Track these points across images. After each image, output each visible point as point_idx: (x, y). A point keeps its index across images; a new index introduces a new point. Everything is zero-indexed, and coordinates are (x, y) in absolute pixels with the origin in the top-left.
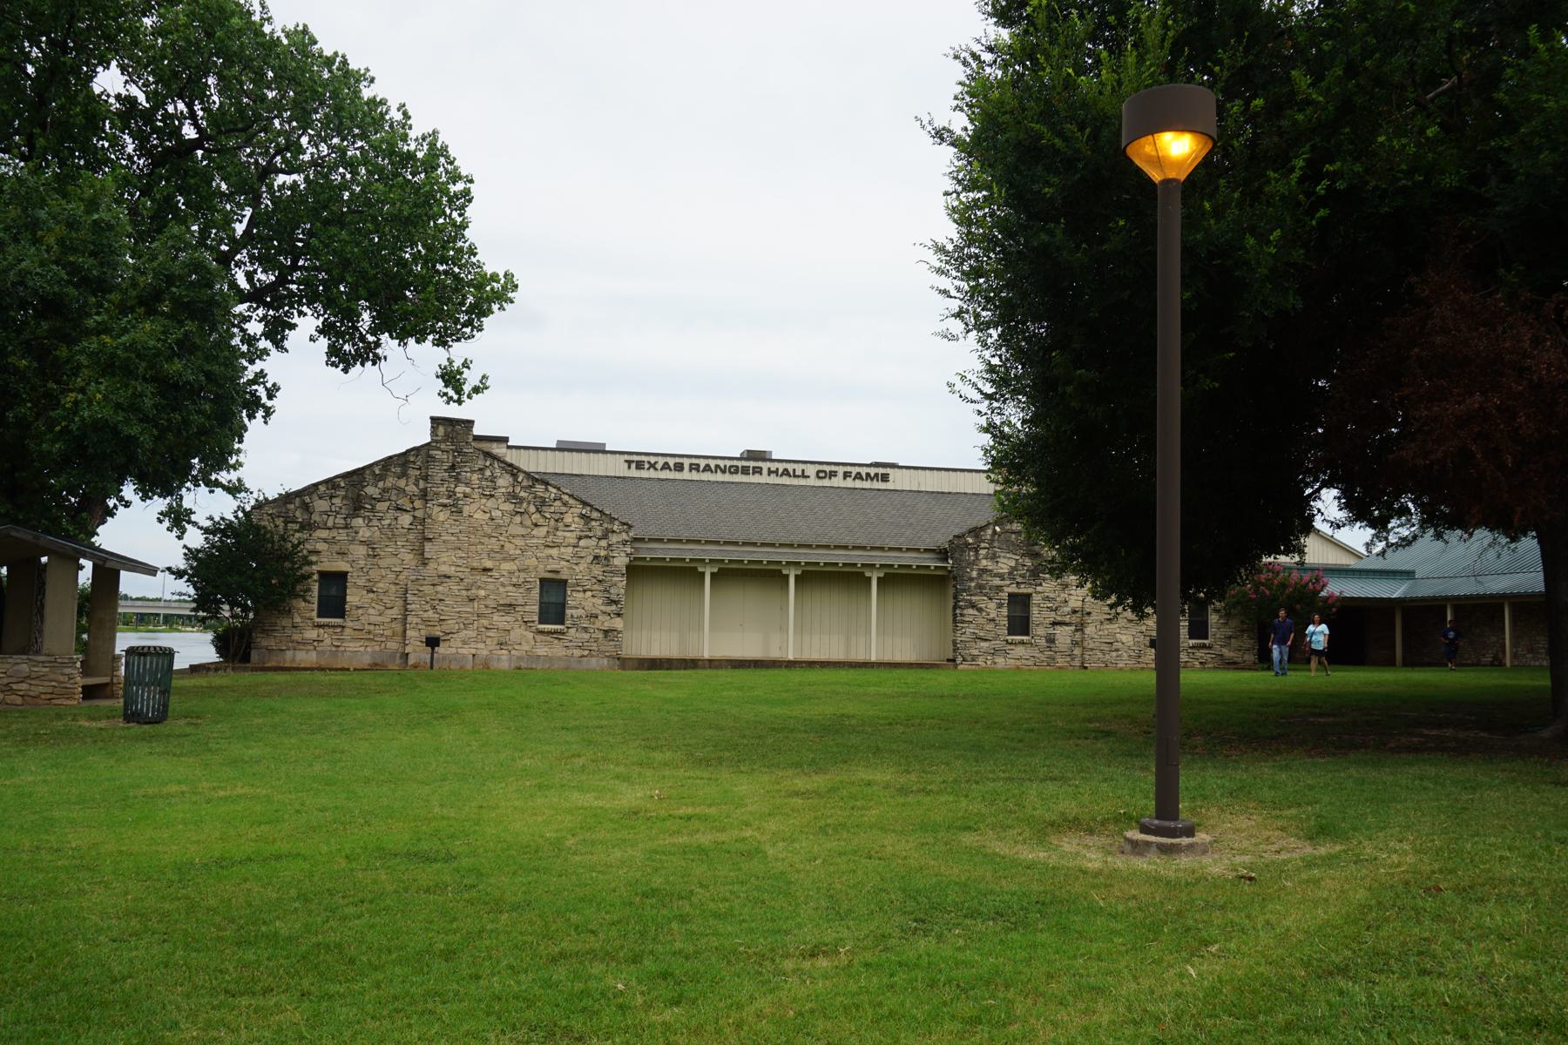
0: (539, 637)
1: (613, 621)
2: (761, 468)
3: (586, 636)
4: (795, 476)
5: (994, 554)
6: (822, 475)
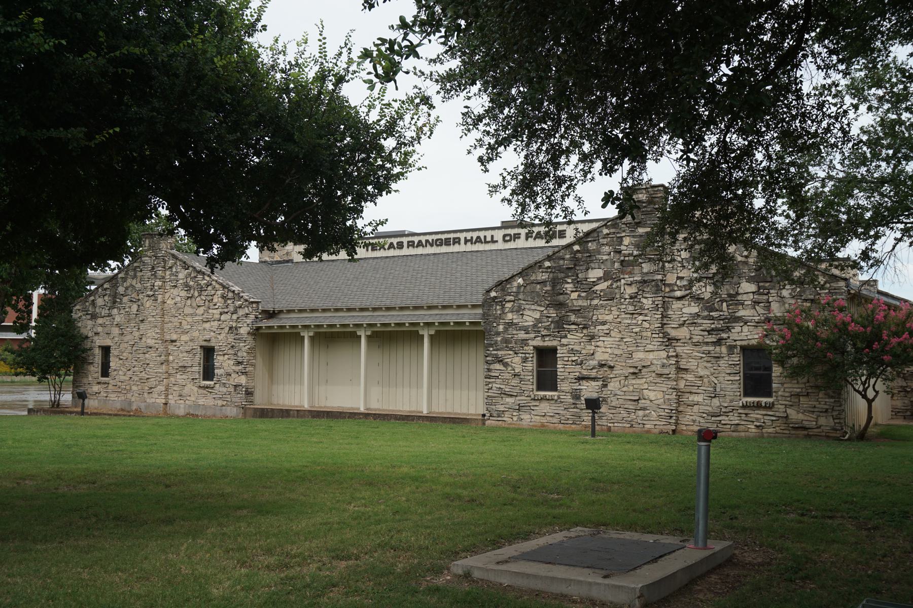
0: (201, 391)
1: (240, 378)
2: (459, 239)
3: (224, 390)
4: (486, 242)
5: (520, 307)
6: (508, 238)
